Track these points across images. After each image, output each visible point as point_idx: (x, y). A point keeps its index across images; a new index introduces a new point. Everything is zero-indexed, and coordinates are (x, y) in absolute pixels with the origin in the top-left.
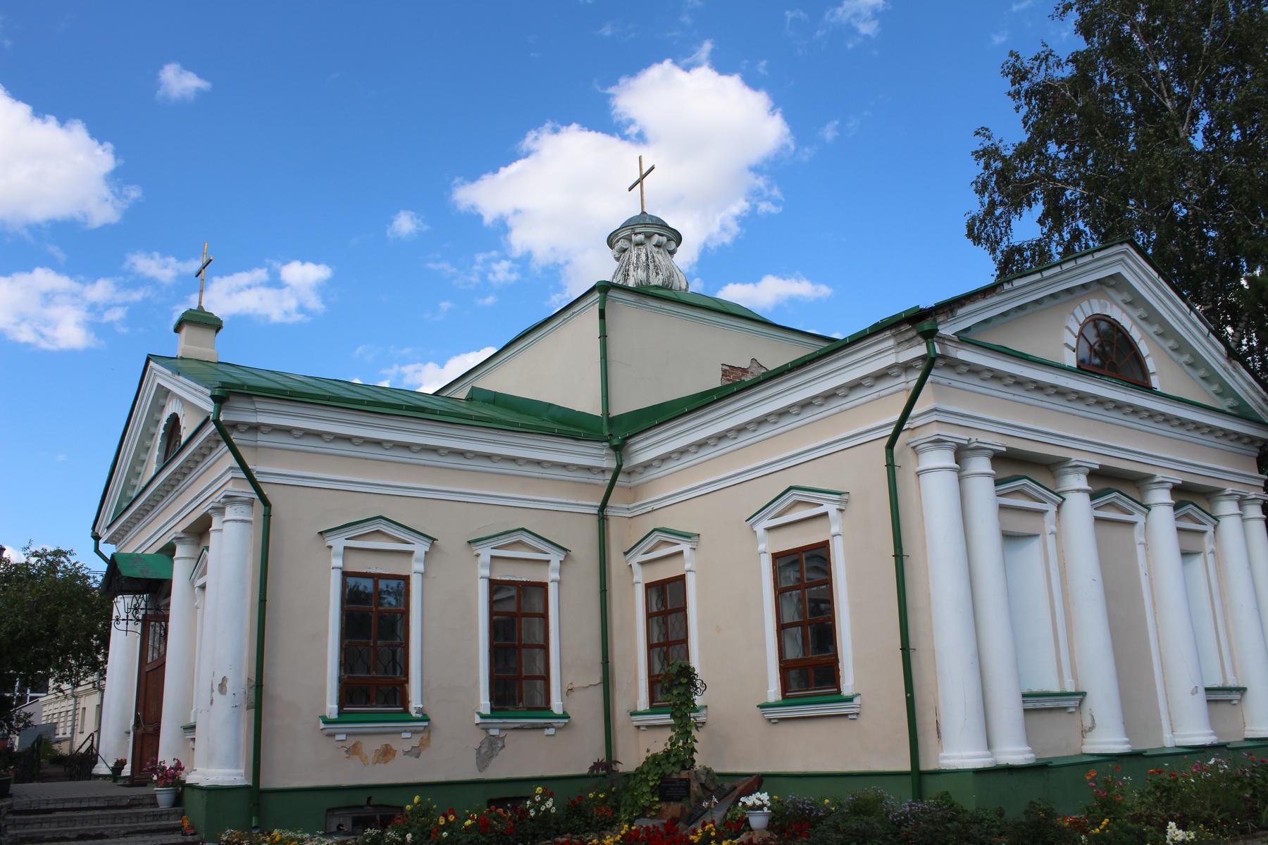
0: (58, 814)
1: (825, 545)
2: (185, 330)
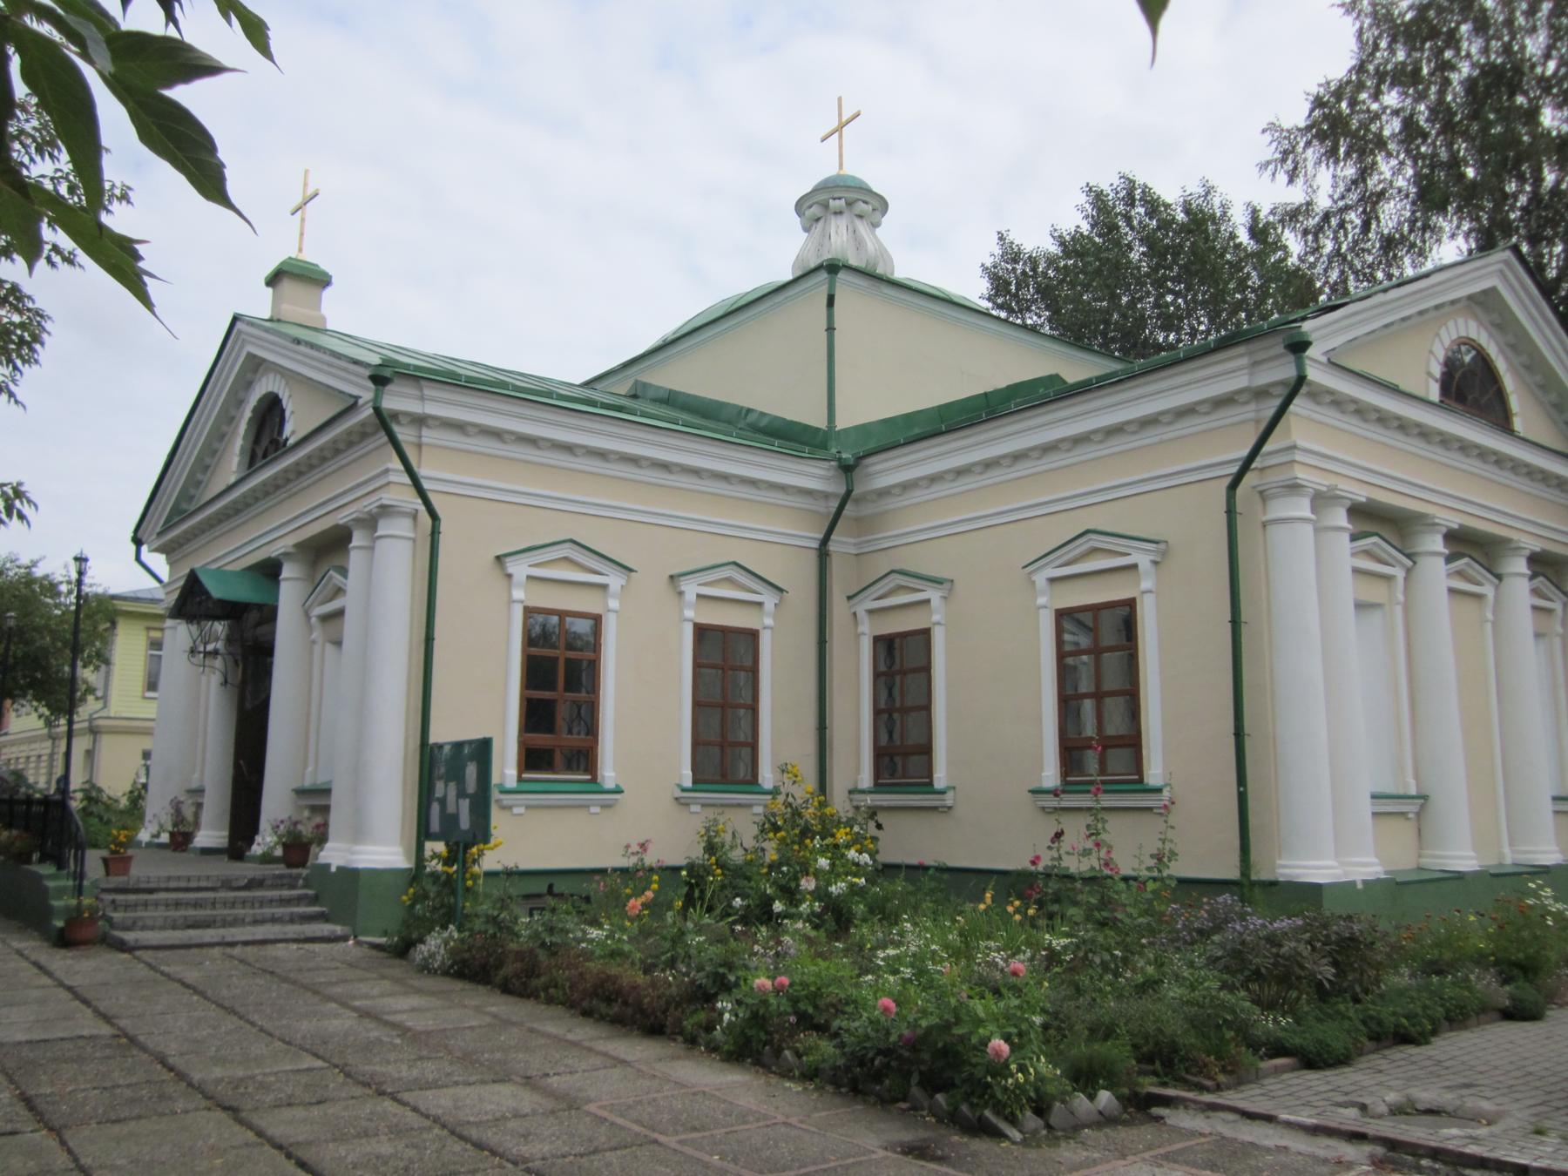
0: (162, 896)
2: (287, 286)
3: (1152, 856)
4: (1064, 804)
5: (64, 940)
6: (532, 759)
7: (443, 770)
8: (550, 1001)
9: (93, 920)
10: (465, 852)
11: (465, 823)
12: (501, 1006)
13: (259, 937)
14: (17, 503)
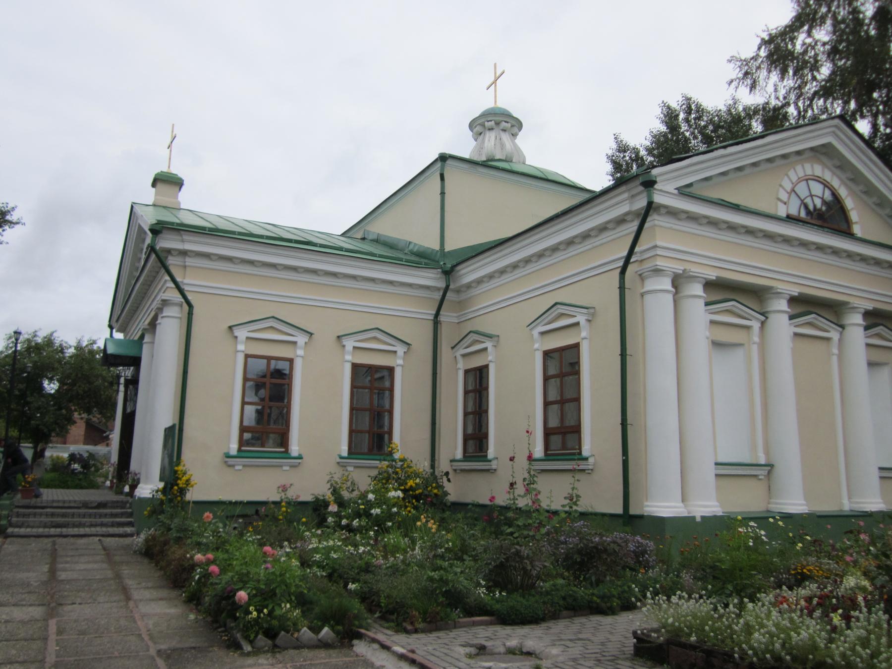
0: (48, 510)
1: (577, 346)
2: (159, 185)
13: (82, 533)
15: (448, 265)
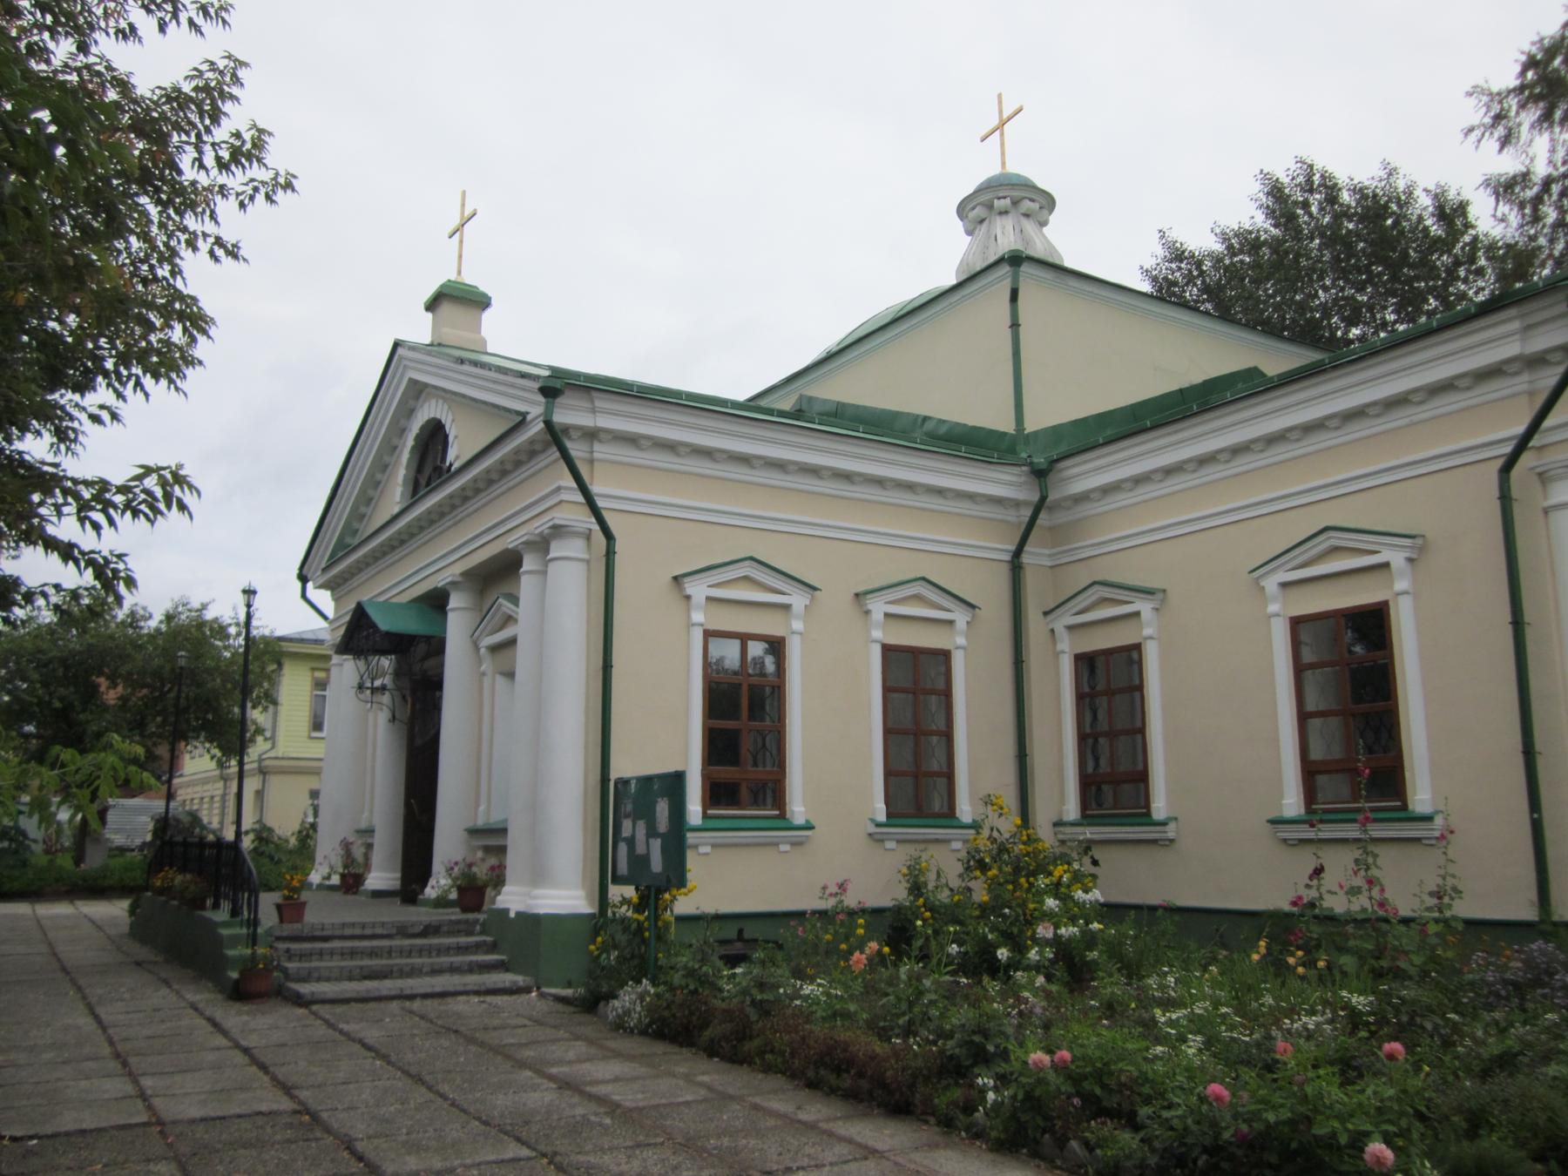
2: (446, 309)
3: (1431, 894)
4: (1322, 835)
5: (240, 993)
6: (717, 793)
7: (629, 807)
8: (767, 1069)
9: (268, 970)
10: (657, 899)
11: (657, 864)
12: (713, 1074)
14: (177, 490)
15: (1041, 458)
